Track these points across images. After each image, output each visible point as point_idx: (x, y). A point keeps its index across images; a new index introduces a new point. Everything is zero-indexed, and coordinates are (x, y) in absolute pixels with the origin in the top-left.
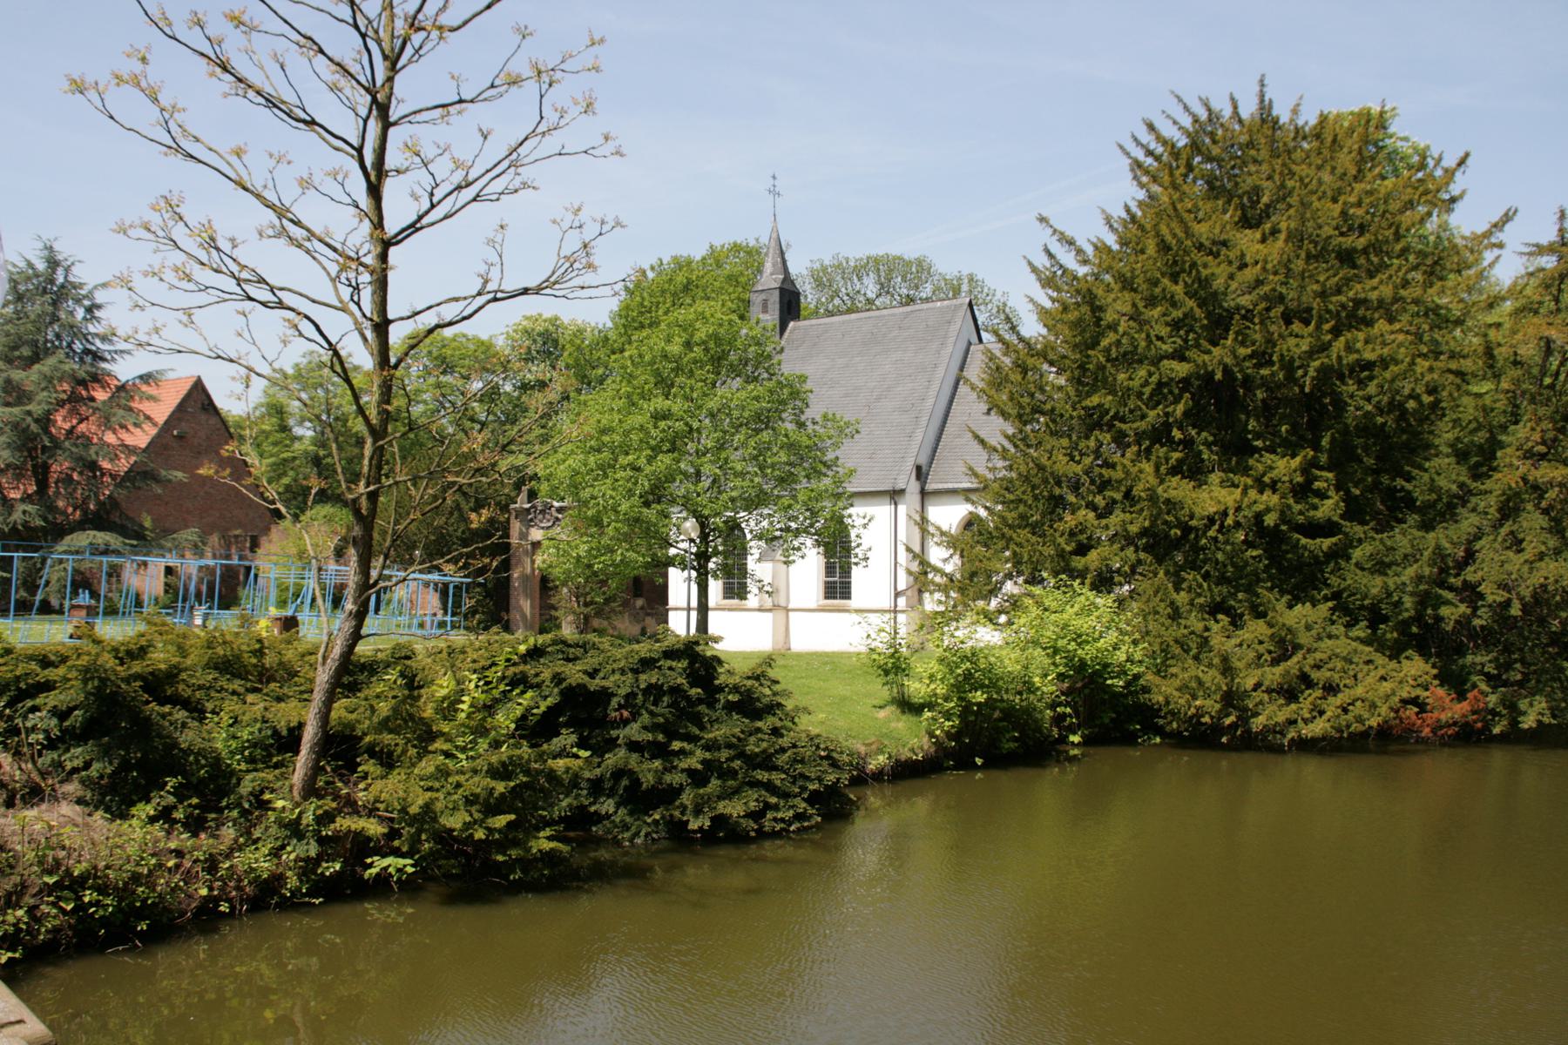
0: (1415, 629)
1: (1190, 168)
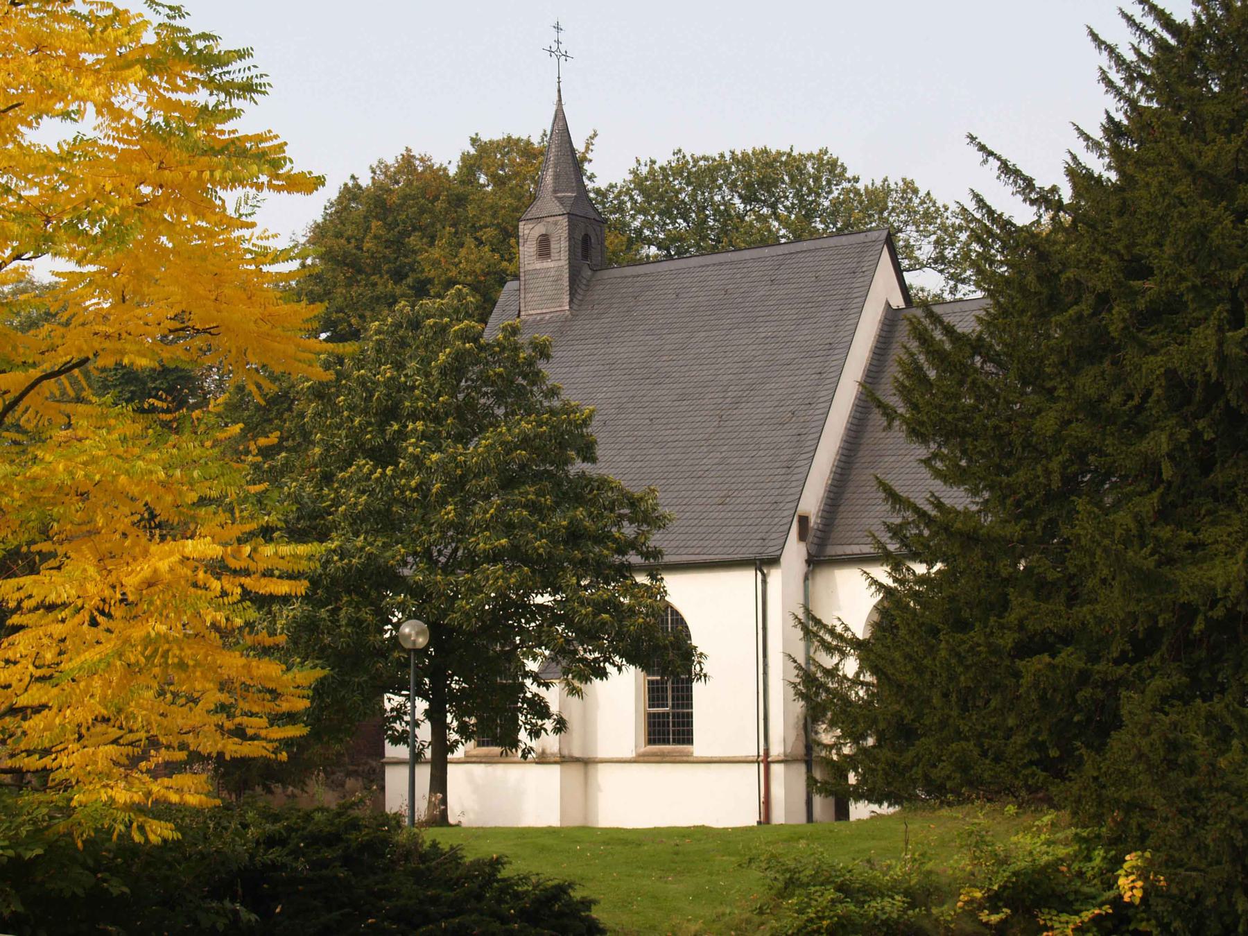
0: (870, 741)
1: (924, 231)
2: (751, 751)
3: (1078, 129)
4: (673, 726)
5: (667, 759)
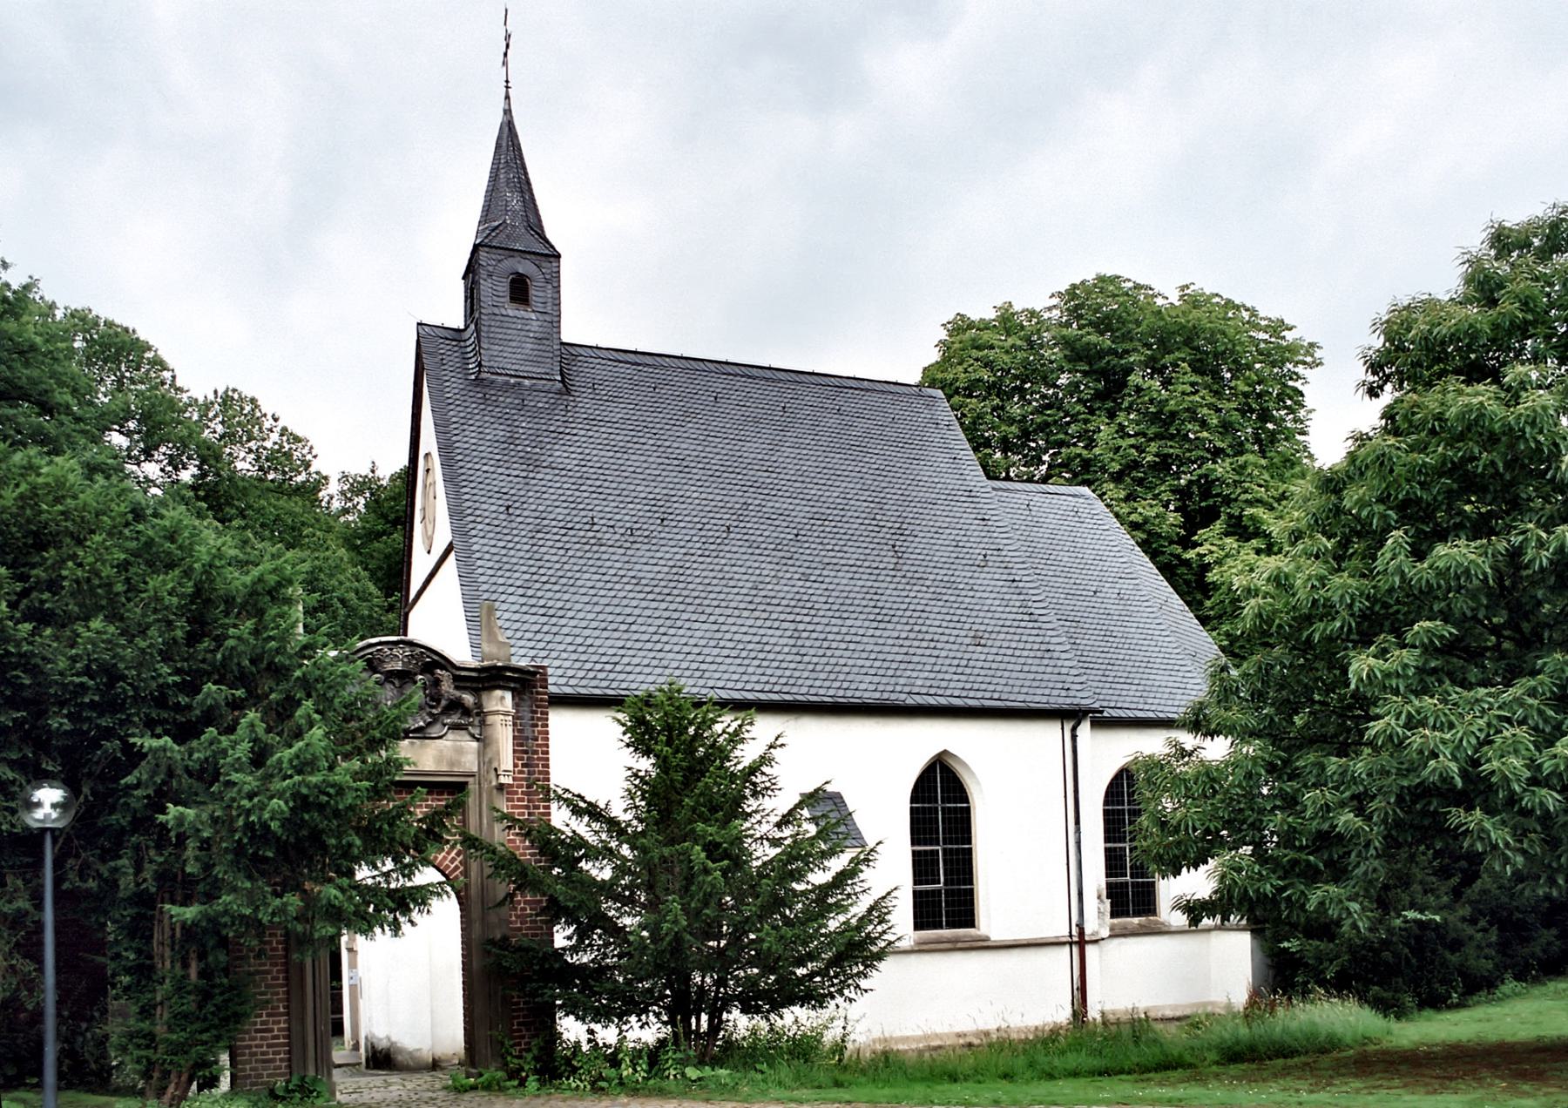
2: (1061, 930)
3: (508, 112)
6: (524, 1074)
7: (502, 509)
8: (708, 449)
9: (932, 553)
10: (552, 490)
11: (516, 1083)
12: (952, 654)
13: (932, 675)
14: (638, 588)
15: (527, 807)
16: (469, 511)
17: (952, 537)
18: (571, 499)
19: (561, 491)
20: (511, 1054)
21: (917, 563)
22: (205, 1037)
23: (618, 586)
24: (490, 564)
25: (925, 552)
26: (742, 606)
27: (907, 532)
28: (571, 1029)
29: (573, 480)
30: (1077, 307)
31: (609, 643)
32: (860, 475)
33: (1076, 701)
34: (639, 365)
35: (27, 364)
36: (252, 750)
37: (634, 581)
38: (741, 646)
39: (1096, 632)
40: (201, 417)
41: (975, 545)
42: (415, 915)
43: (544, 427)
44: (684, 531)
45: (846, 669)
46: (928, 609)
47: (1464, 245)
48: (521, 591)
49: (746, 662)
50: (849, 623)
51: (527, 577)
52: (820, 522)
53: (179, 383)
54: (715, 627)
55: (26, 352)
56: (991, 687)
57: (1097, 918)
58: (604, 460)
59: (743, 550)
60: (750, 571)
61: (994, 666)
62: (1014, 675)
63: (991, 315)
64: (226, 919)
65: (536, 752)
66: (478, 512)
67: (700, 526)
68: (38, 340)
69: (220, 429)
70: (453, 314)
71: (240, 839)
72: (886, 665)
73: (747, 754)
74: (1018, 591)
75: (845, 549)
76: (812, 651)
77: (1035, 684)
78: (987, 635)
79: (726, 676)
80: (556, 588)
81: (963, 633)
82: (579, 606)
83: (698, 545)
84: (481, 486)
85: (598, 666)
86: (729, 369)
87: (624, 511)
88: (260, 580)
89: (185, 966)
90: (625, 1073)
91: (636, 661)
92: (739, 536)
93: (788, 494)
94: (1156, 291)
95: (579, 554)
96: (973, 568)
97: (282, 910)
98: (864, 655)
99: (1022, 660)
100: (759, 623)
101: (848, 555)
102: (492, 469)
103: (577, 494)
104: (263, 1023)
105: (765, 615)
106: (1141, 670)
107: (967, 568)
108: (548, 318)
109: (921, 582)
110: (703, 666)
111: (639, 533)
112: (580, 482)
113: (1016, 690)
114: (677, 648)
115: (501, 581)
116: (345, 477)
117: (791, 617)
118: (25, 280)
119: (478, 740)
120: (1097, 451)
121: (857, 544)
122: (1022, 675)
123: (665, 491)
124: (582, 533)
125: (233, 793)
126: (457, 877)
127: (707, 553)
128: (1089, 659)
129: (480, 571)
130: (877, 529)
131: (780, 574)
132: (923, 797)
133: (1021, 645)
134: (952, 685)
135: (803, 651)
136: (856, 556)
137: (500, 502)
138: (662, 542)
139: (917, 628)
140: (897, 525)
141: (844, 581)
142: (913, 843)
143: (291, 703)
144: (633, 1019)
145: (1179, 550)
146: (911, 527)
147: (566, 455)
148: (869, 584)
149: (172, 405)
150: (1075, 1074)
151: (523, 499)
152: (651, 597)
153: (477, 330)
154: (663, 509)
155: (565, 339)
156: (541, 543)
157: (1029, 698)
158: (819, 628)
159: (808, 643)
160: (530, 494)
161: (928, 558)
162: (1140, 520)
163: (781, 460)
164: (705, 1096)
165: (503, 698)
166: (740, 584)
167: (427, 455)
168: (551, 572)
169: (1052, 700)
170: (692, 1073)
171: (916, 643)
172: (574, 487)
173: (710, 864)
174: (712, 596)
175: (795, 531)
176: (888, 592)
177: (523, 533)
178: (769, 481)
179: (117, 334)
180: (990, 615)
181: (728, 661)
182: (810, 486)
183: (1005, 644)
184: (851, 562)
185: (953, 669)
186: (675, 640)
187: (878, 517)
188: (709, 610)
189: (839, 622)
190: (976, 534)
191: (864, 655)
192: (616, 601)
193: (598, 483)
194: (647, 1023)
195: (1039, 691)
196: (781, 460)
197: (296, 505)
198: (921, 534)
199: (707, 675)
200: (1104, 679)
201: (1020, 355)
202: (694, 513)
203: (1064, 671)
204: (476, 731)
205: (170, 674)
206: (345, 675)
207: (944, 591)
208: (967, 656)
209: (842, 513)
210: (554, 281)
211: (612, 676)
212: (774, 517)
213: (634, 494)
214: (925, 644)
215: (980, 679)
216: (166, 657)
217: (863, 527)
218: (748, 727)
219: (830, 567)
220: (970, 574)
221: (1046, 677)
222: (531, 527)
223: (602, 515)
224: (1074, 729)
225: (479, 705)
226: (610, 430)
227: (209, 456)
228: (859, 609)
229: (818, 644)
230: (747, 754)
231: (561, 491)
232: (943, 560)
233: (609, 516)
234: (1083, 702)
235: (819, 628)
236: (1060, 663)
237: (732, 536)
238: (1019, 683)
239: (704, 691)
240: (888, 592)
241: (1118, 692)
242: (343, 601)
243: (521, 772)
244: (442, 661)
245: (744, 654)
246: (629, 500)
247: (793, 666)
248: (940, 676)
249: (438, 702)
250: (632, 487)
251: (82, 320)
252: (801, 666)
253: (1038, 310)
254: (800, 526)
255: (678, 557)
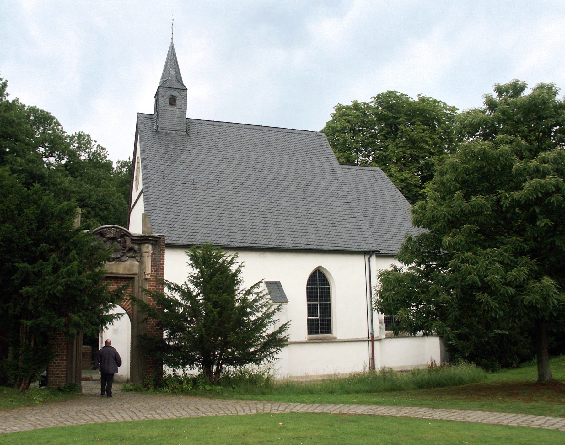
2: (365, 335)
3: (172, 43)
4: (321, 325)
5: (325, 341)
6: (149, 386)
7: (161, 177)
8: (237, 155)
9: (318, 192)
10: (180, 170)
11: (146, 389)
12: (323, 230)
13: (315, 238)
14: (208, 205)
15: (155, 286)
16: (149, 178)
17: (326, 186)
18: (186, 173)
19: (183, 170)
20: (145, 378)
21: (312, 196)
22: (34, 367)
23: (200, 205)
24: (155, 197)
25: (315, 192)
26: (246, 211)
27: (309, 185)
28: (168, 370)
29: (187, 166)
30: (380, 102)
31: (196, 225)
32: (293, 164)
33: (370, 248)
34: (214, 125)
35: (12, 127)
36: (53, 268)
37: (207, 202)
38: (244, 226)
39: (381, 221)
40: (70, 142)
41: (334, 189)
42: (107, 325)
43: (179, 148)
44: (226, 184)
45: (283, 235)
46: (315, 213)
47: (484, 92)
48: (165, 206)
49: (246, 232)
50: (285, 218)
51: (168, 201)
52: (277, 181)
53: (64, 130)
54: (235, 219)
55: (11, 123)
56: (338, 242)
57: (379, 330)
58: (199, 159)
59: (248, 191)
60: (250, 199)
61: (339, 234)
62: (347, 237)
63: (350, 104)
64: (41, 326)
65: (160, 266)
66: (153, 178)
67: (232, 182)
68: (15, 119)
69: (76, 145)
70: (151, 110)
71: (46, 299)
72: (298, 233)
73: (233, 268)
74: (350, 206)
75: (285, 191)
76: (271, 228)
77: (354, 241)
78: (337, 223)
79: (238, 237)
80: (178, 205)
81: (328, 222)
82: (185, 212)
83: (231, 189)
84: (154, 169)
85: (191, 234)
86: (247, 126)
87: (205, 177)
88: (62, 208)
89: (30, 341)
90: (184, 387)
91: (205, 232)
92: (247, 186)
93: (265, 171)
94: (409, 96)
95: (188, 193)
96: (333, 198)
97: (59, 323)
98: (290, 230)
99: (349, 232)
100: (252, 218)
101: (286, 193)
102: (159, 163)
103: (189, 171)
104: (58, 363)
105: (254, 215)
106: (397, 236)
107: (331, 198)
108: (182, 110)
109: (313, 203)
110: (230, 234)
111: (210, 185)
112: (190, 167)
113: (347, 243)
114: (220, 227)
115: (159, 203)
116: (119, 162)
117: (264, 216)
118: (14, 99)
119: (139, 262)
120: (388, 153)
121: (290, 189)
122: (350, 238)
123: (220, 170)
124: (189, 185)
125: (45, 283)
126: (130, 311)
127: (234, 192)
128: (377, 232)
129: (151, 199)
130: (298, 183)
131: (261, 200)
132: (312, 283)
133: (350, 226)
134: (323, 241)
135: (267, 228)
136: (289, 193)
137: (161, 174)
138: (218, 188)
139: (310, 220)
140: (305, 182)
141: (284, 203)
142: (307, 301)
143: (68, 251)
144: (188, 366)
145: (418, 190)
146: (311, 183)
147: (185, 157)
148: (294, 203)
149: (60, 138)
150: (357, 392)
151: (169, 173)
152: (212, 208)
153: (158, 115)
154: (219, 177)
155: (188, 117)
156: (174, 189)
157: (352, 246)
158: (274, 220)
159: (269, 225)
160: (172, 171)
161: (316, 194)
162: (403, 178)
163: (264, 158)
164: (210, 396)
165: (148, 247)
166: (246, 203)
167: (138, 157)
168: (177, 199)
169: (361, 247)
170: (208, 387)
171: (310, 226)
172: (188, 169)
173: (213, 309)
174: (235, 208)
175: (267, 184)
176: (301, 207)
177: (168, 185)
178: (258, 166)
179: (44, 114)
180: (338, 215)
181: (239, 232)
182: (274, 168)
183: (344, 226)
184: (287, 196)
185: (323, 235)
186: (220, 224)
187: (298, 179)
188: (233, 213)
189: (282, 218)
190: (335, 185)
191: (290, 230)
192: (199, 210)
193: (196, 167)
194: (193, 368)
195: (356, 244)
196: (264, 158)
197: (101, 172)
198: (314, 185)
199: (231, 237)
200: (383, 239)
201: (361, 118)
202: (230, 178)
203: (366, 236)
204: (138, 259)
205: (30, 241)
206: (87, 241)
207: (322, 206)
208: (329, 230)
209: (285, 177)
210: (185, 98)
211: (196, 237)
212: (260, 179)
213: (209, 171)
214: (313, 226)
215: (333, 239)
216: (29, 235)
217: (293, 183)
218: (235, 258)
219: (279, 197)
220: (332, 200)
221: (359, 238)
222: (171, 183)
223: (197, 179)
224: (369, 258)
225: (140, 249)
226: (202, 149)
227: (72, 155)
228: (289, 213)
229: (273, 226)
230: (233, 268)
231: (183, 170)
232: (322, 195)
233: (199, 179)
234: (373, 248)
235: (274, 220)
236: (364, 233)
237: (244, 186)
238: (349, 240)
239: (229, 243)
240: (301, 207)
241: (388, 244)
242: (113, 206)
243: (154, 274)
244: (127, 234)
245: (245, 229)
246: (207, 173)
247: (263, 234)
248: (319, 238)
249: (125, 248)
250: (209, 169)
251: (33, 110)
252: (266, 234)
253: (367, 102)
254: (269, 182)
255: (223, 194)
